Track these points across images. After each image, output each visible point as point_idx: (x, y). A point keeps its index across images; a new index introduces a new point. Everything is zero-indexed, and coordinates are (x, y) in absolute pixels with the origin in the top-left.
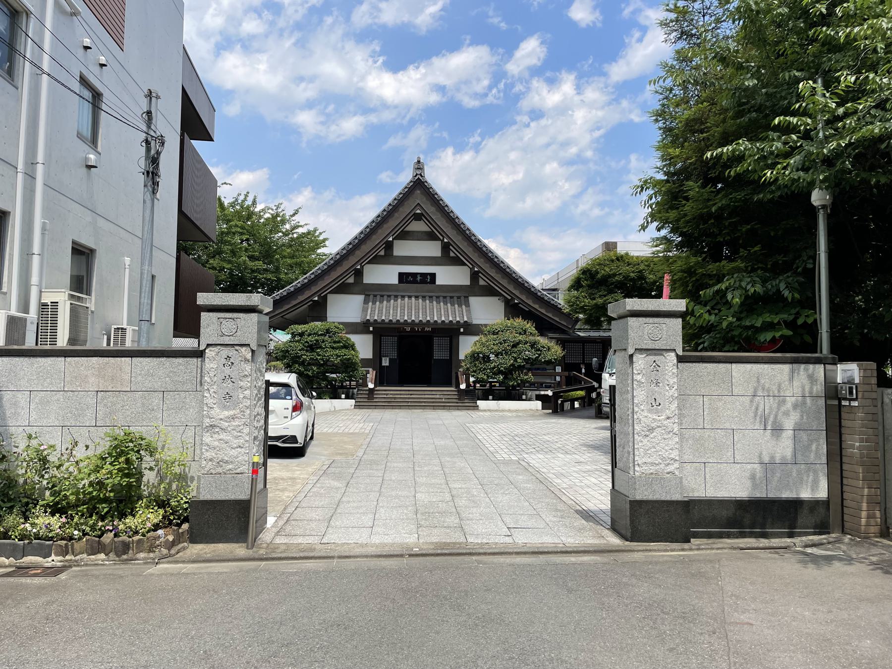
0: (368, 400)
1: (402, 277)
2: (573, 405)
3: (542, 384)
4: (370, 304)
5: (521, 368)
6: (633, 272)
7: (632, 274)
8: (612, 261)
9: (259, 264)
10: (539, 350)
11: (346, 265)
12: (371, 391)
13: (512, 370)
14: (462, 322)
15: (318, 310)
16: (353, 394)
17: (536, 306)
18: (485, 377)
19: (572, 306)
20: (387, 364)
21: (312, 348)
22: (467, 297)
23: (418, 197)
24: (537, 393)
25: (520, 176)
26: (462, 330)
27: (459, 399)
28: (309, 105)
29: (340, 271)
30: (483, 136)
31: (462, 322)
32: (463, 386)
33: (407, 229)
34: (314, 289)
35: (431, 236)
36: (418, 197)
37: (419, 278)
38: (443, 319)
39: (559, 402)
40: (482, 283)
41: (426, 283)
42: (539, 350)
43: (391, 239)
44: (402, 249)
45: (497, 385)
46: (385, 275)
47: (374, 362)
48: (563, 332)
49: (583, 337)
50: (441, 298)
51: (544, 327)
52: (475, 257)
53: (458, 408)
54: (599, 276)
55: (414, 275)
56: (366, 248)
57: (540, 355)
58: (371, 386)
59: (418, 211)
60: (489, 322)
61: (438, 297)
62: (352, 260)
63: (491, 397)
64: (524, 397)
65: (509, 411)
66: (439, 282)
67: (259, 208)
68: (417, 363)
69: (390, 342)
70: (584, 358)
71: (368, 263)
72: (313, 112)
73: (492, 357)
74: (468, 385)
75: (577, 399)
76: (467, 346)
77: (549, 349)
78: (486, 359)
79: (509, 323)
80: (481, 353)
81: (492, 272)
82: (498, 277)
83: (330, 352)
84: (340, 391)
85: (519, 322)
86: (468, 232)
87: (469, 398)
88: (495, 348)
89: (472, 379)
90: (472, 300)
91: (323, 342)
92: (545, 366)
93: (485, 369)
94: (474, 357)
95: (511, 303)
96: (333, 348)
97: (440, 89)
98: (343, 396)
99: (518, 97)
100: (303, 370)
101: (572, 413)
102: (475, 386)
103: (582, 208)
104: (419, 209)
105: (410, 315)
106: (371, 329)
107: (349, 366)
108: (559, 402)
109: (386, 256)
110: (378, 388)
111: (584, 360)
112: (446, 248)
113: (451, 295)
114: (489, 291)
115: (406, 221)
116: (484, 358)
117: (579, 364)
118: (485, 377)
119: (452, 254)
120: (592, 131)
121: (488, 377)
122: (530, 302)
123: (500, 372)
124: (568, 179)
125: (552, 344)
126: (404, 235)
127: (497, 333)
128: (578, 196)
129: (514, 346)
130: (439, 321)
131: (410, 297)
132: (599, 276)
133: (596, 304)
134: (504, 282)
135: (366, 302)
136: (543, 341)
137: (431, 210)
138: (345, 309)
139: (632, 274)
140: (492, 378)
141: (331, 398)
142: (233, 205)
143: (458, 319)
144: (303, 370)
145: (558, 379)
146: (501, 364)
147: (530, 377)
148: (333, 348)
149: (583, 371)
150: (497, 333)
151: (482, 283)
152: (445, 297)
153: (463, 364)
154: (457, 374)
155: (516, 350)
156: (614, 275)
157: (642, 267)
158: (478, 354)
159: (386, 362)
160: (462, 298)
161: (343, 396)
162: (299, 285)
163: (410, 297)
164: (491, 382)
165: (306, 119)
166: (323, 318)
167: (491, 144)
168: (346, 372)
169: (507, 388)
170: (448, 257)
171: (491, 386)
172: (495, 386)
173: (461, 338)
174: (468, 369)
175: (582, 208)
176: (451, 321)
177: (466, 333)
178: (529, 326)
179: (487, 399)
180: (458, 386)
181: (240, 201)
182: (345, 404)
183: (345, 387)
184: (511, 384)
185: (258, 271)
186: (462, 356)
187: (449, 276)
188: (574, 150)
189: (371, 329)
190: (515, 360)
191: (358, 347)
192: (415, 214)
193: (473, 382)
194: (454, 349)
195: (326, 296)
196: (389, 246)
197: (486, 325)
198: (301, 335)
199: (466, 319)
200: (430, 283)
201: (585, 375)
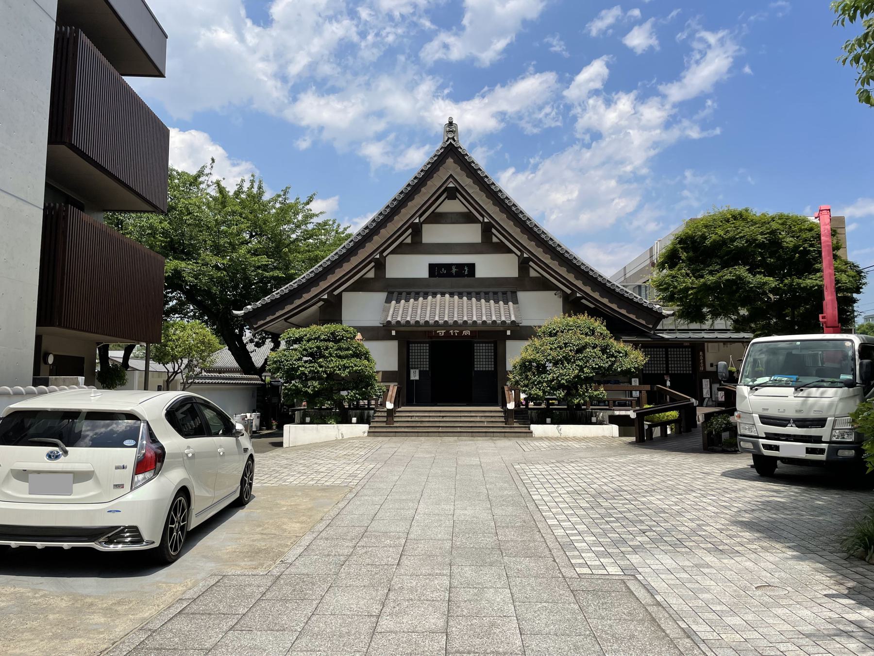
0: (389, 426)
1: (434, 269)
2: (664, 431)
3: (614, 402)
4: (394, 302)
5: (588, 380)
6: (762, 233)
7: (759, 237)
8: (728, 221)
9: (264, 260)
10: (613, 356)
11: (362, 254)
12: (390, 413)
13: (576, 383)
14: (508, 322)
15: (331, 310)
16: (369, 416)
17: (605, 301)
18: (541, 393)
19: (666, 289)
20: (417, 378)
21: (315, 355)
22: (514, 293)
23: (451, 166)
24: (610, 413)
25: (575, 194)
26: (509, 333)
27: (506, 423)
28: (379, 137)
29: (355, 261)
30: (543, 157)
31: (508, 322)
32: (511, 406)
33: (439, 210)
34: (323, 285)
35: (467, 218)
36: (451, 166)
37: (454, 270)
38: (484, 318)
39: (646, 427)
40: (533, 274)
41: (463, 276)
42: (613, 356)
43: (417, 221)
44: (432, 234)
45: (556, 402)
46: (414, 266)
47: (399, 376)
48: (642, 333)
49: (668, 339)
50: (482, 294)
51: (618, 327)
52: (524, 239)
53: (504, 435)
54: (708, 242)
55: (448, 266)
56: (386, 233)
57: (613, 363)
58: (390, 406)
59: (451, 185)
60: (545, 323)
61: (478, 293)
62: (370, 247)
63: (548, 420)
64: (594, 419)
65: (575, 439)
66: (480, 273)
67: (266, 197)
68: (453, 377)
69: (422, 353)
70: (667, 367)
71: (392, 252)
72: (381, 144)
73: (549, 366)
74: (518, 403)
75: (669, 422)
76: (516, 353)
77: (626, 355)
78: (541, 369)
79: (571, 320)
80: (534, 360)
81: (547, 259)
82: (554, 264)
83: (334, 363)
84: (351, 412)
85: (583, 320)
86: (514, 209)
87: (524, 418)
88: (554, 353)
89: (523, 396)
90: (521, 295)
91: (327, 348)
92: (621, 378)
93: (540, 382)
94: (525, 366)
95: (571, 299)
96: (340, 357)
97: (502, 116)
98: (354, 420)
99: (575, 119)
100: (300, 386)
101: (663, 444)
102: (527, 405)
103: (636, 223)
104: (452, 179)
105: (442, 314)
106: (394, 333)
107: (361, 382)
108: (646, 427)
109: (416, 246)
110: (403, 408)
111: (667, 370)
112: (487, 230)
113: (495, 290)
114: (543, 285)
115: (436, 198)
116: (538, 367)
117: (664, 374)
118: (541, 393)
119: (495, 240)
120: (649, 148)
121: (544, 392)
122: (596, 295)
123: (560, 386)
124: (624, 194)
125: (628, 348)
126: (437, 218)
127: (555, 335)
128: (634, 214)
129: (579, 351)
130: (479, 322)
131: (443, 294)
132: (708, 242)
133: (705, 284)
134: (563, 271)
135: (388, 301)
136: (618, 346)
137: (466, 182)
138: (363, 309)
139: (759, 237)
140: (549, 394)
141: (338, 423)
142: (237, 194)
143: (503, 319)
144: (300, 386)
145: (636, 394)
146: (561, 375)
147: (601, 392)
148: (340, 357)
149: (668, 383)
150: (555, 335)
151: (533, 274)
152: (486, 293)
153: (511, 376)
154: (503, 388)
155: (581, 356)
156: (733, 240)
157: (774, 225)
158: (530, 362)
159: (415, 376)
160: (509, 294)
161: (354, 420)
162: (304, 281)
163: (443, 294)
164: (548, 400)
165: (374, 151)
166: (339, 321)
167: (547, 165)
168: (356, 388)
169: (570, 408)
170: (490, 244)
171: (548, 404)
172: (553, 404)
173: (509, 344)
174: (517, 382)
175: (636, 223)
176: (494, 322)
177: (513, 337)
178: (599, 326)
179: (545, 423)
180: (504, 404)
181: (245, 189)
182: (357, 430)
183: (358, 407)
184: (576, 401)
185: (265, 268)
186: (509, 367)
187: (491, 267)
188: (629, 168)
189: (394, 333)
190: (581, 369)
191: (373, 355)
192: (447, 189)
193: (525, 399)
194: (499, 358)
195: (340, 294)
196: (417, 231)
197: (540, 327)
198: (298, 340)
199: (513, 318)
200: (468, 276)
201: (670, 387)
